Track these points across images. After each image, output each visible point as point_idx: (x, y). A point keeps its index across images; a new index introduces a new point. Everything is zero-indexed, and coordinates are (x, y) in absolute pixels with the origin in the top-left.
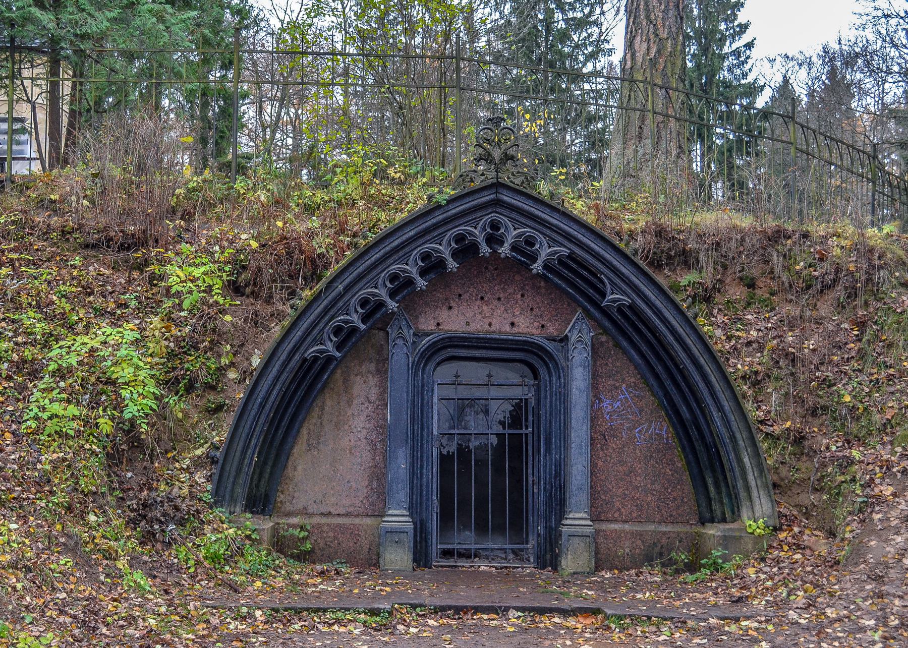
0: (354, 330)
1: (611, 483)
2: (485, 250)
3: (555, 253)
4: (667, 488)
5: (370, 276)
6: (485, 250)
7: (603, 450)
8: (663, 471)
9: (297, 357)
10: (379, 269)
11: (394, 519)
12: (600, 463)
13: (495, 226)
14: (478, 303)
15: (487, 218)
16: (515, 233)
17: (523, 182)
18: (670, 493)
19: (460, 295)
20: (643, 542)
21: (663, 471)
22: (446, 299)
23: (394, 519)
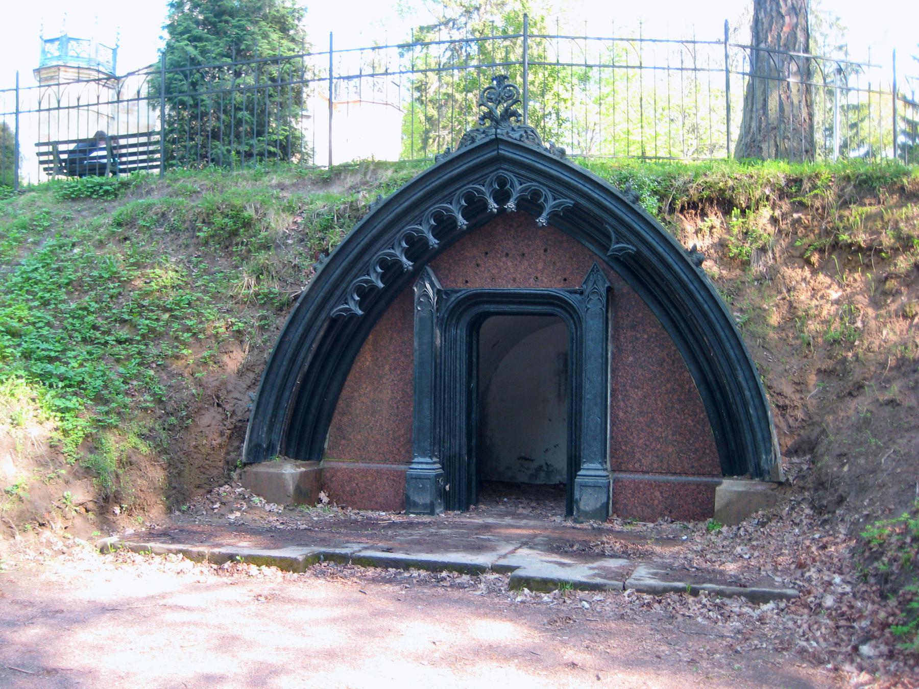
0: (374, 288)
1: (632, 434)
2: (493, 206)
3: (559, 205)
4: (689, 439)
5: (386, 237)
6: (493, 206)
7: (623, 401)
8: (685, 422)
9: (323, 316)
10: (394, 231)
11: (420, 466)
12: (621, 414)
13: (502, 182)
14: (504, 259)
15: (534, 185)
16: (520, 187)
17: (521, 136)
18: (691, 445)
19: (487, 253)
20: (661, 493)
21: (685, 422)
22: (474, 257)
23: (420, 466)
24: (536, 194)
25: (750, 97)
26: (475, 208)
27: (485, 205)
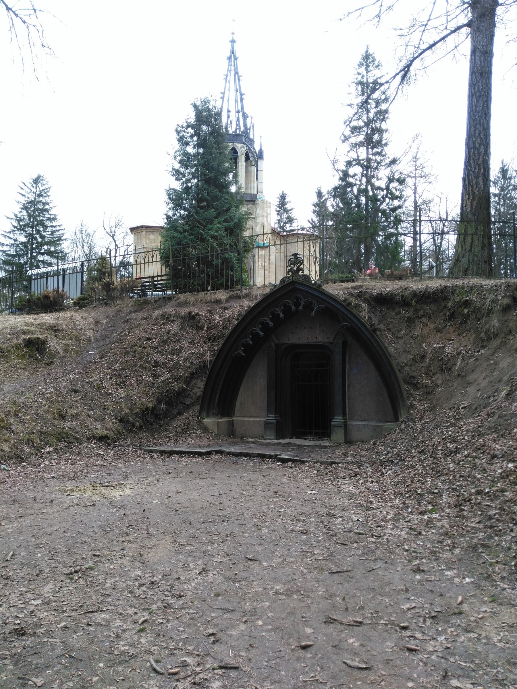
2: (294, 308)
6: (294, 308)
13: (297, 298)
24: (311, 303)
25: (320, 270)
26: (287, 310)
27: (291, 308)
